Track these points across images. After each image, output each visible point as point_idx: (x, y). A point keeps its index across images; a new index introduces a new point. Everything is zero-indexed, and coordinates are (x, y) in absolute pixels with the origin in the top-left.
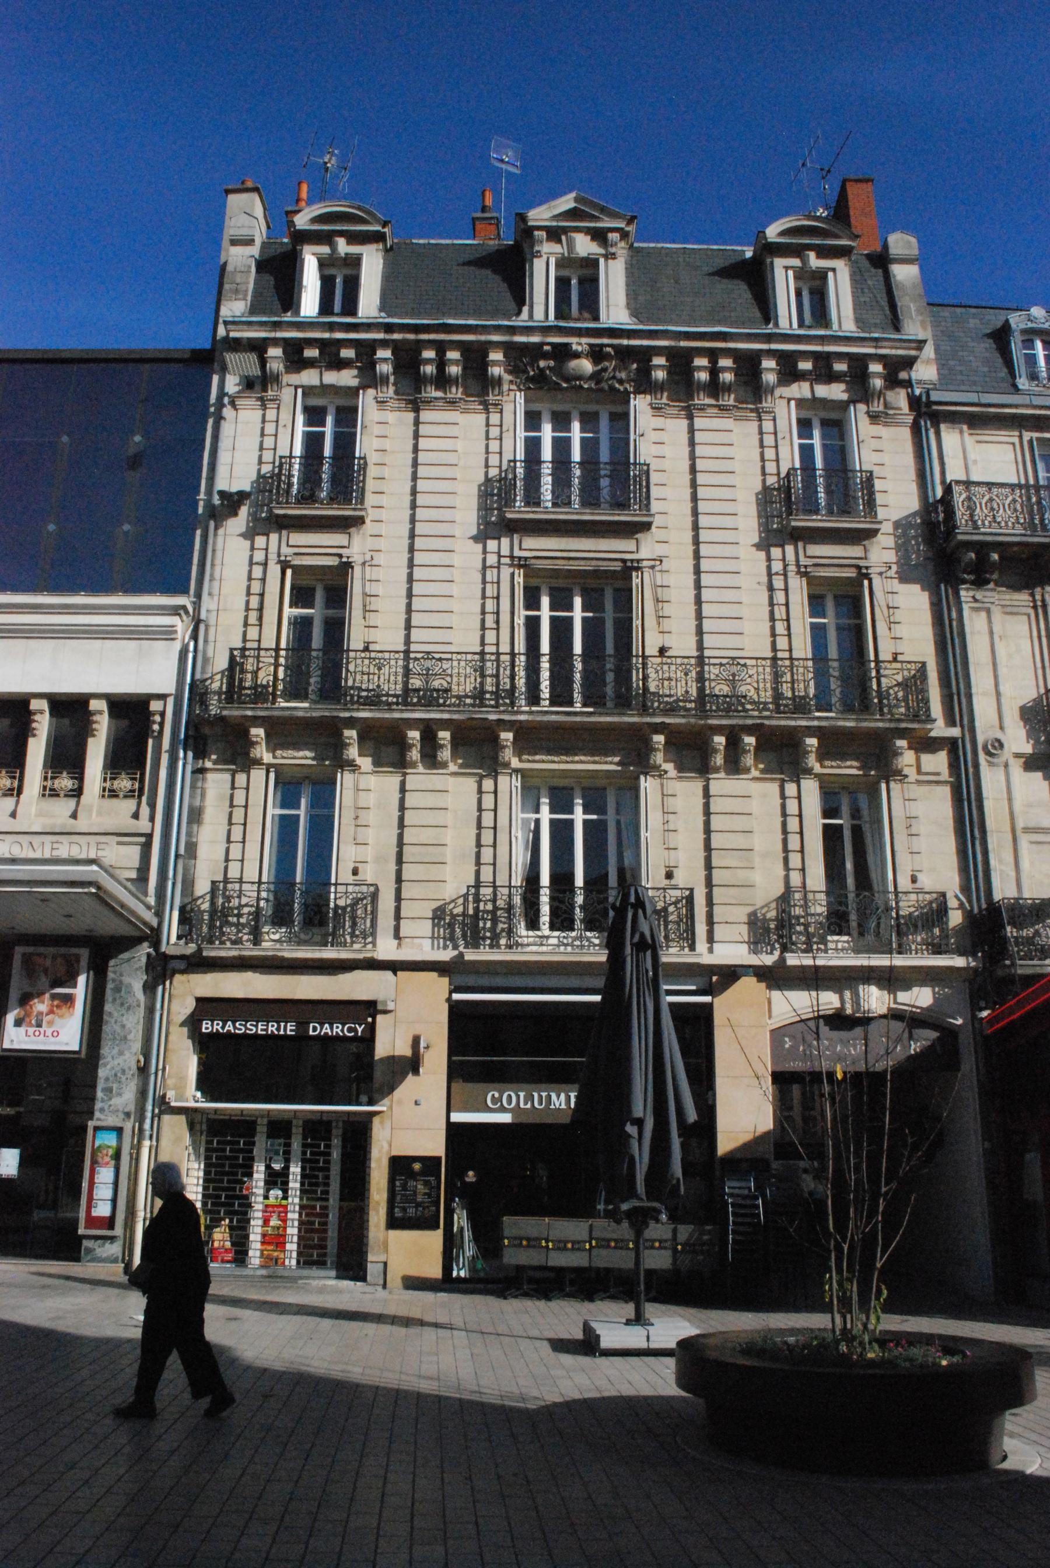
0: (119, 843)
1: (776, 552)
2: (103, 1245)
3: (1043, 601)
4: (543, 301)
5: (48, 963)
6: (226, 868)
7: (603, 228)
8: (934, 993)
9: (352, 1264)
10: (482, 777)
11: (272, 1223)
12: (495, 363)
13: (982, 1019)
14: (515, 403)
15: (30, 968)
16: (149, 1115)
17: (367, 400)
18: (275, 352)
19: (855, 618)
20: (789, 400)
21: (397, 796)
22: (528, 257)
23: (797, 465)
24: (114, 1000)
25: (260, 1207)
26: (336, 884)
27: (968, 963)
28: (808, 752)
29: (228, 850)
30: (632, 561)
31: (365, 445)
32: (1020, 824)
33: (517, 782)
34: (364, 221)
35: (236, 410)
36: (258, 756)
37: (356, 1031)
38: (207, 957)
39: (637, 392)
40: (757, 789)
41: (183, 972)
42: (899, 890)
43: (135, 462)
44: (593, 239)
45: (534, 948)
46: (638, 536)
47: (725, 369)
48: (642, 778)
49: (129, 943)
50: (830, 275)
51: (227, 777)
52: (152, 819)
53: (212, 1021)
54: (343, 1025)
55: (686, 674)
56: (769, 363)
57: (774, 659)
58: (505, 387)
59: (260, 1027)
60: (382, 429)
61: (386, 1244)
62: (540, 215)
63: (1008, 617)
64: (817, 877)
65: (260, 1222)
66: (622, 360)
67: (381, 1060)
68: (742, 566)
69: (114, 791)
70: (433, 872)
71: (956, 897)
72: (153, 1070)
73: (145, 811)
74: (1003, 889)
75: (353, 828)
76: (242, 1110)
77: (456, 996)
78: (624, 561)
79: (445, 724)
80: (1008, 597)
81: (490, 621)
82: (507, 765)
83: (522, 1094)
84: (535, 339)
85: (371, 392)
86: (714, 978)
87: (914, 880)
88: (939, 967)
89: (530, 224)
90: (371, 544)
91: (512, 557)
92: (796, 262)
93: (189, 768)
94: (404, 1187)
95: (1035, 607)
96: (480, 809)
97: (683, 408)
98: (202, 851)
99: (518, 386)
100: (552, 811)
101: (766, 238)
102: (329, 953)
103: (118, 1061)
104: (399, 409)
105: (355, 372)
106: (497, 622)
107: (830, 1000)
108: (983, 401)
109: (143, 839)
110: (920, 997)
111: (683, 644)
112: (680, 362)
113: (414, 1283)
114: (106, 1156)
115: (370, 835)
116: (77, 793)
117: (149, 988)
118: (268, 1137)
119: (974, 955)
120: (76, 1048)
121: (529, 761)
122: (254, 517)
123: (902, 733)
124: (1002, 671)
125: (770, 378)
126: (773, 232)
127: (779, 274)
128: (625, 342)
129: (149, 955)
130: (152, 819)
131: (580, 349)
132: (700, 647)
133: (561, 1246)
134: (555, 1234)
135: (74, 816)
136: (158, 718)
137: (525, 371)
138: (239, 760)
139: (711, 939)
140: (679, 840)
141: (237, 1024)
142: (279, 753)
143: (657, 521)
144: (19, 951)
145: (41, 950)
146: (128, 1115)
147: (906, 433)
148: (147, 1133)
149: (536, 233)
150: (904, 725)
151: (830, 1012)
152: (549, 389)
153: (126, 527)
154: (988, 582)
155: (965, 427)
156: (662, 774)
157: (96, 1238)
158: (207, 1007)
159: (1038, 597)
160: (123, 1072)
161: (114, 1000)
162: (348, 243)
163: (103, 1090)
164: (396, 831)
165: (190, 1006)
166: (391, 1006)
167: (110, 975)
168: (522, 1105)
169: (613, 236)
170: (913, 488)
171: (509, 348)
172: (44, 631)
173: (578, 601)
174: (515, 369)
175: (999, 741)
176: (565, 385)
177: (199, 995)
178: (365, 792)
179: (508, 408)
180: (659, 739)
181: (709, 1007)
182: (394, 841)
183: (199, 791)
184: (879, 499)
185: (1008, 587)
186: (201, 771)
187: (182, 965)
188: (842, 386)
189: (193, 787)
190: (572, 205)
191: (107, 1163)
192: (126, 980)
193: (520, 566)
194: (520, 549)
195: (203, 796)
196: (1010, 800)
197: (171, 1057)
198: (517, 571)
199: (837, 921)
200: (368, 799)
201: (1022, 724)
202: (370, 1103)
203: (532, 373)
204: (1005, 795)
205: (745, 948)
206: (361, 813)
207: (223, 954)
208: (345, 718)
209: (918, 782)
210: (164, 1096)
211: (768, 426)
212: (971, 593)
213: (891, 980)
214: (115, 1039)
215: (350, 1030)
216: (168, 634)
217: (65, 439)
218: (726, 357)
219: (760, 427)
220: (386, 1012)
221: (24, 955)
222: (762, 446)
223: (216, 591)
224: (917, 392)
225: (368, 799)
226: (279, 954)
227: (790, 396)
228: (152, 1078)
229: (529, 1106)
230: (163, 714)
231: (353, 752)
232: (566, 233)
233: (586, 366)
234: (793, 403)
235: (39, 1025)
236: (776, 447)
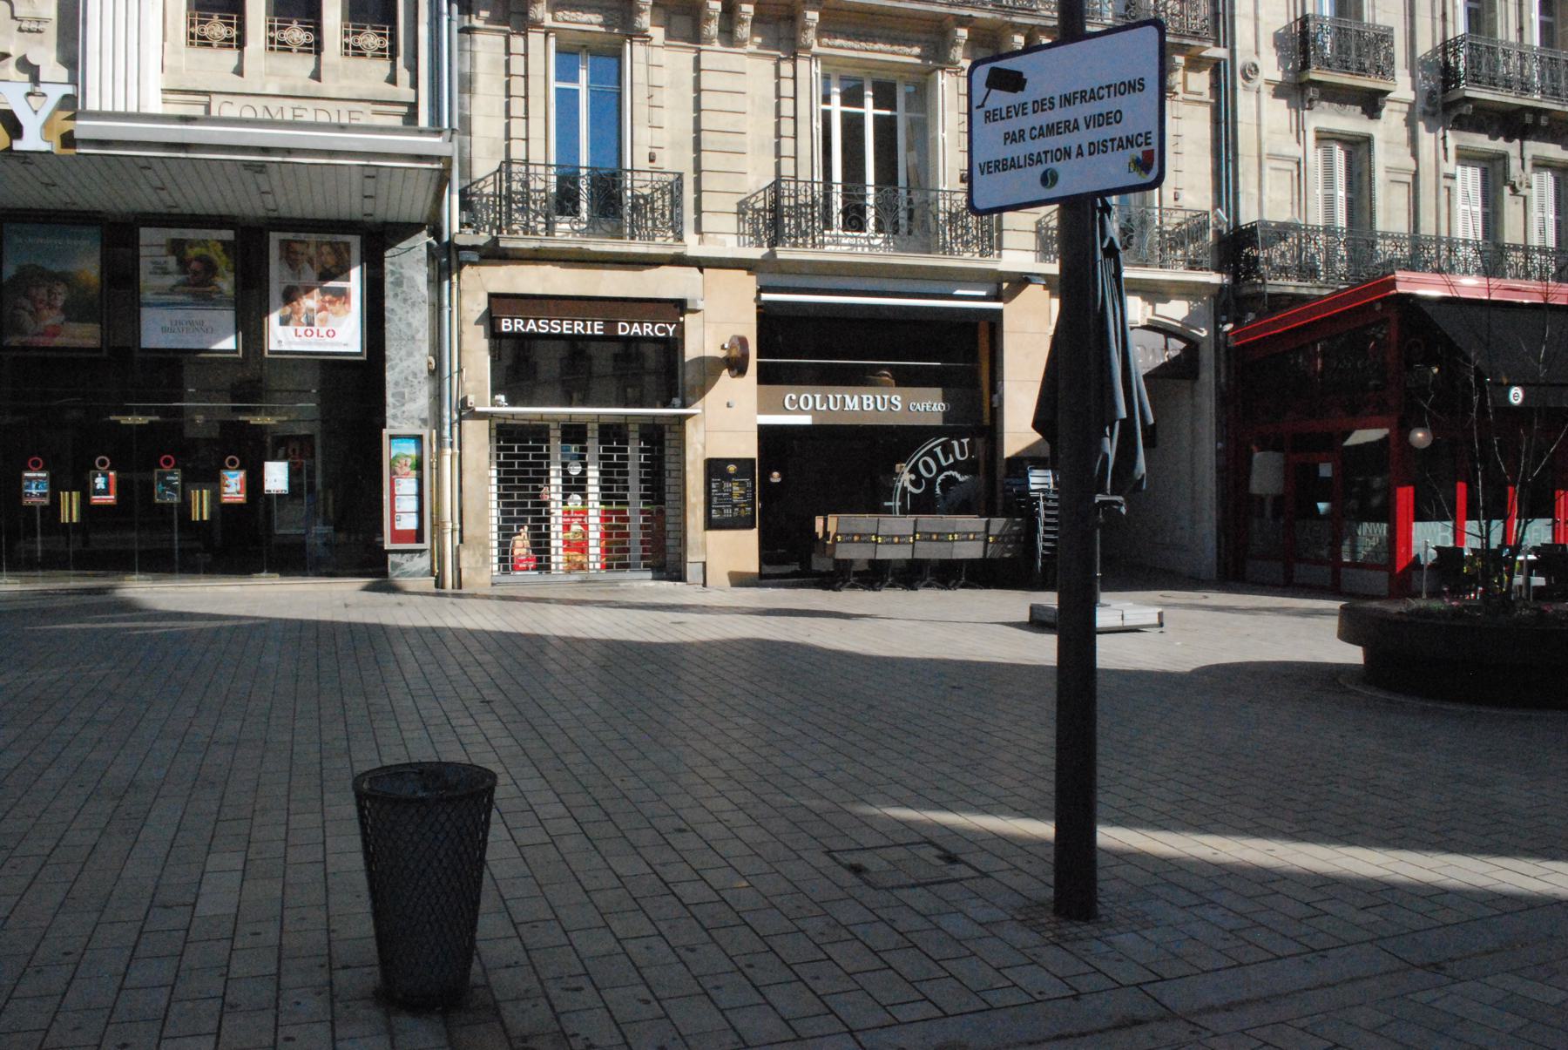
5: (312, 251)
6: (508, 148)
9: (669, 566)
10: (780, 59)
15: (290, 255)
16: (447, 421)
21: (691, 75)
24: (396, 295)
25: (559, 513)
26: (632, 171)
29: (508, 127)
32: (1265, 150)
33: (817, 69)
38: (505, 249)
40: (749, 64)
41: (473, 264)
45: (832, 248)
49: (406, 230)
51: (501, 39)
52: (415, 84)
54: (654, 324)
61: (704, 544)
67: (691, 361)
70: (733, 162)
72: (447, 373)
73: (403, 75)
76: (542, 415)
77: (765, 297)
83: (818, 396)
86: (1005, 285)
94: (720, 488)
96: (778, 96)
98: (478, 125)
102: (638, 247)
103: (405, 366)
109: (405, 109)
110: (1176, 311)
113: (739, 580)
114: (406, 467)
117: (436, 282)
120: (358, 350)
129: (429, 245)
130: (415, 84)
135: (239, 71)
138: (513, 19)
142: (559, 14)
144: (275, 238)
145: (302, 236)
146: (424, 421)
148: (448, 440)
157: (403, 552)
158: (500, 303)
160: (415, 375)
161: (396, 295)
164: (692, 115)
165: (483, 305)
166: (700, 305)
167: (388, 267)
177: (492, 291)
180: (963, 33)
181: (999, 313)
182: (691, 126)
186: (468, 31)
187: (475, 257)
189: (461, 50)
192: (407, 272)
195: (473, 59)
197: (466, 358)
202: (684, 406)
205: (1032, 255)
206: (656, 91)
207: (523, 245)
210: (464, 401)
214: (401, 339)
215: (660, 330)
220: (695, 311)
221: (282, 242)
226: (585, 247)
235: (310, 324)
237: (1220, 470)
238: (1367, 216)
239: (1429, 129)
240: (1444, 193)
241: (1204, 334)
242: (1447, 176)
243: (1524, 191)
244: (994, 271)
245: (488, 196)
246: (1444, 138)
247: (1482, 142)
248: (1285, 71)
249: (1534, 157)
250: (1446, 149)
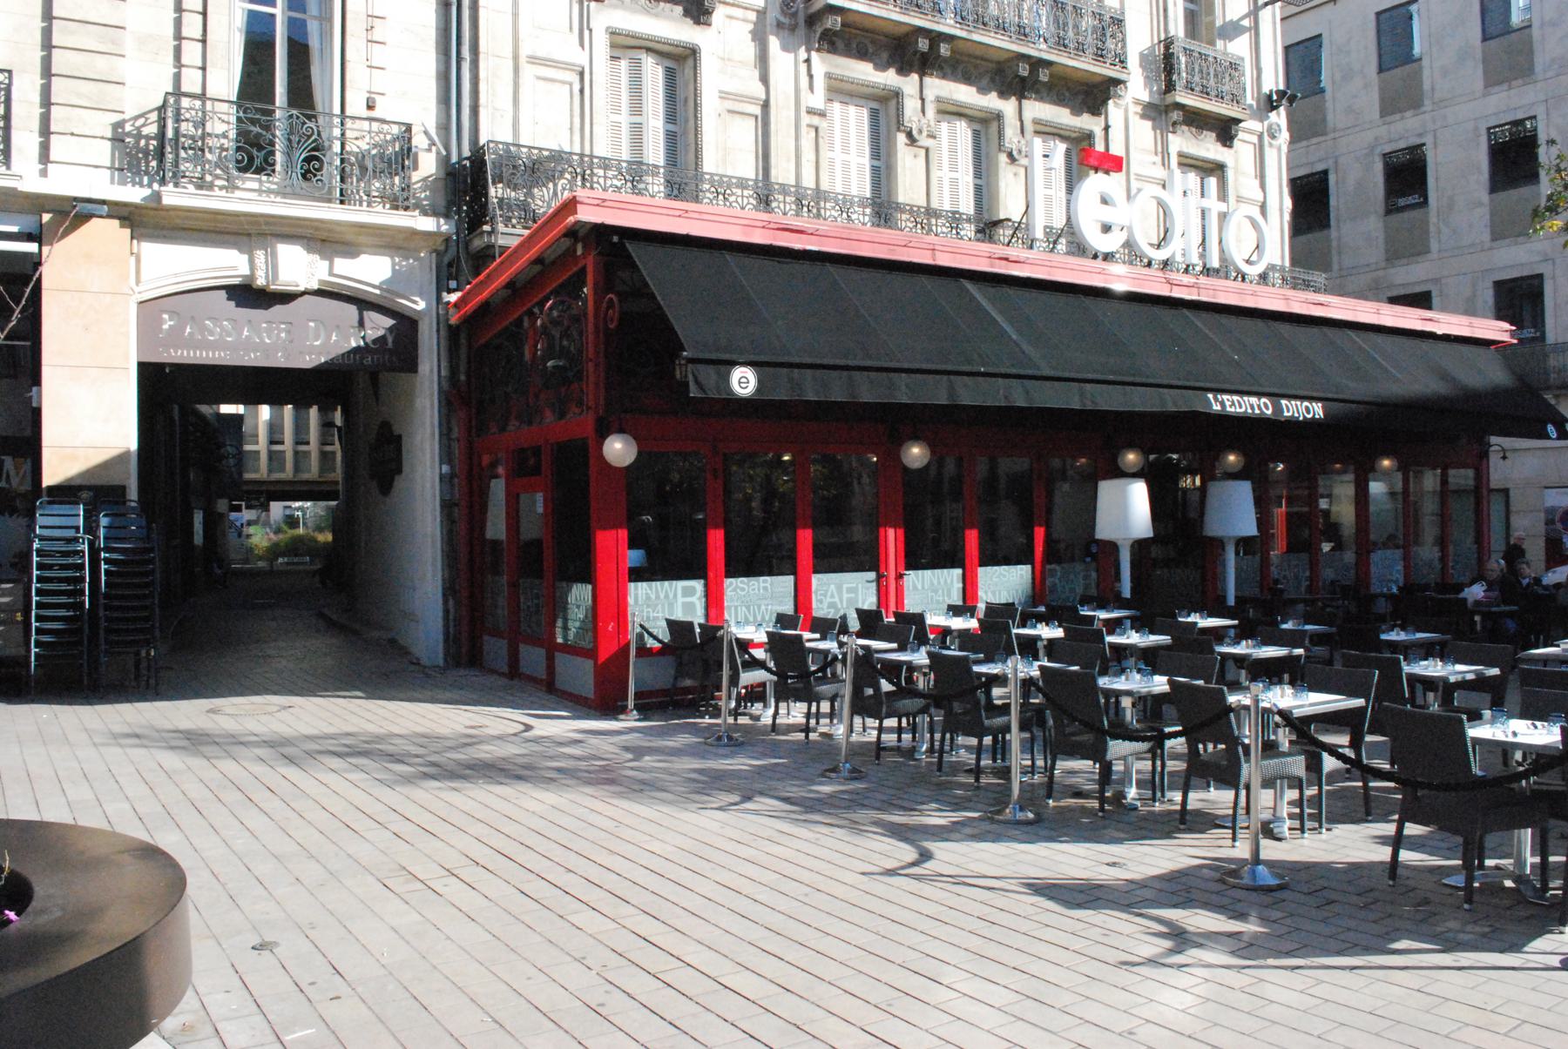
8: (394, 265)
13: (448, 303)
27: (439, 226)
32: (524, 51)
42: (348, 113)
71: (426, 133)
74: (494, 129)
107: (229, 263)
110: (370, 271)
119: (447, 216)
139: (45, 156)
151: (236, 281)
181: (36, 262)
199: (253, 154)
213: (323, 240)
237: (447, 506)
238: (692, 156)
239: (785, 48)
240: (808, 139)
241: (421, 305)
242: (811, 112)
243: (924, 141)
244: (15, 189)
245: (148, 138)
246: (808, 61)
247: (863, 71)
248: (1151, 91)
249: (939, 100)
250: (811, 76)
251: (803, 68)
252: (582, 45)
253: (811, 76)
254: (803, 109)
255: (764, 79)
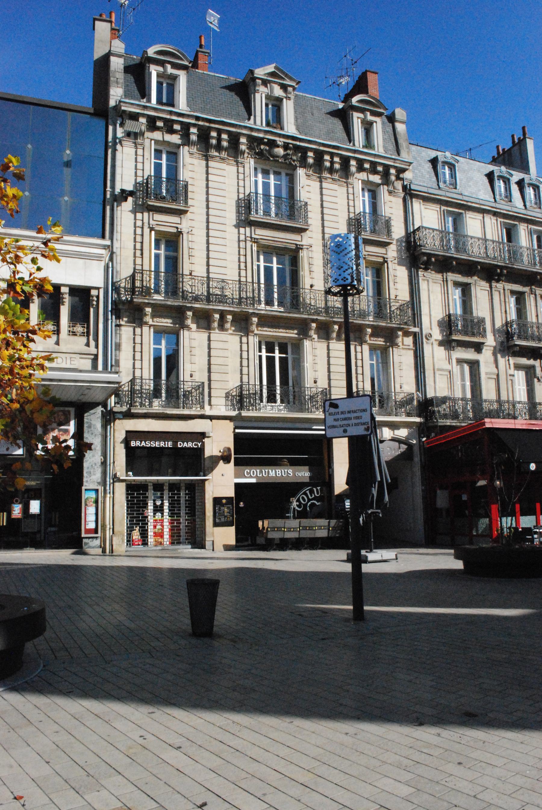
0: (81, 358)
1: (139, 216)
2: (93, 541)
3: (446, 279)
4: (260, 115)
7: (285, 84)
10: (242, 336)
11: (157, 527)
12: (243, 144)
14: (250, 163)
16: (108, 483)
17: (184, 151)
18: (143, 120)
19: (174, 252)
20: (151, 140)
22: (253, 91)
23: (153, 174)
24: (88, 432)
25: (152, 521)
28: (253, 324)
30: (300, 245)
31: (184, 175)
32: (436, 367)
34: (182, 59)
35: (122, 146)
36: (147, 321)
37: (198, 445)
39: (300, 167)
43: (68, 164)
44: (281, 88)
46: (302, 234)
47: (336, 162)
48: (305, 340)
49: (93, 405)
50: (375, 124)
51: (131, 329)
52: (97, 347)
53: (136, 441)
54: (193, 443)
55: (202, 285)
56: (353, 163)
57: (240, 281)
58: (246, 155)
59: (157, 444)
60: (191, 166)
61: (213, 533)
62: (260, 72)
63: (434, 284)
64: (148, 373)
65: (152, 527)
66: (295, 151)
68: (226, 235)
69: (74, 332)
73: (92, 343)
75: (189, 356)
78: (296, 245)
79: (230, 312)
80: (434, 275)
81: (243, 265)
82: (253, 332)
83: (258, 471)
84: (261, 135)
85: (186, 148)
87: (191, 376)
88: (295, 418)
89: (255, 75)
90: (191, 223)
91: (251, 238)
92: (362, 116)
93: (114, 324)
94: (220, 510)
95: (443, 281)
96: (241, 350)
97: (319, 177)
98: (122, 363)
99: (251, 156)
100: (280, 353)
101: (351, 103)
104: (199, 159)
105: (179, 137)
106: (246, 267)
108: (430, 192)
109: (93, 357)
110: (403, 433)
111: (200, 271)
112: (319, 156)
113: (227, 548)
115: (196, 359)
116: (58, 332)
117: (105, 427)
118: (169, 491)
121: (261, 330)
122: (135, 203)
123: (400, 329)
124: (432, 306)
125: (353, 169)
126: (151, 52)
127: (355, 119)
128: (298, 143)
129: (102, 411)
130: (97, 347)
131: (280, 144)
132: (208, 272)
133: (289, 530)
134: (287, 525)
135: (57, 343)
136: (95, 299)
137: (254, 149)
140: (318, 367)
141: (147, 442)
143: (310, 228)
147: (400, 201)
149: (257, 81)
150: (402, 326)
152: (265, 159)
153: (66, 198)
154: (428, 269)
155: (421, 201)
156: (312, 340)
158: (131, 435)
159: (445, 277)
161: (88, 432)
162: (172, 68)
163: (87, 473)
165: (123, 436)
166: (211, 435)
168: (258, 475)
169: (290, 89)
170: (403, 226)
171: (250, 138)
172: (81, 255)
173: (275, 259)
174: (250, 148)
175: (430, 334)
176: (271, 159)
177: (128, 429)
178: (193, 339)
179: (247, 166)
180: (314, 325)
182: (207, 363)
183: (118, 335)
184: (190, 195)
185: (436, 272)
188: (379, 177)
190: (273, 70)
191: (92, 505)
192: (93, 422)
193: (255, 242)
194: (255, 234)
196: (433, 357)
198: (253, 244)
200: (318, 352)
201: (438, 328)
202: (204, 476)
203: (257, 151)
204: (431, 356)
208: (189, 307)
209: (403, 349)
211: (140, 152)
212: (423, 273)
215: (195, 445)
216: (99, 258)
217: (29, 146)
218: (225, 134)
219: (136, 152)
222: (136, 161)
223: (119, 238)
224: (405, 183)
225: (194, 344)
227: (152, 138)
228: (108, 467)
229: (261, 475)
230: (98, 297)
231: (189, 322)
232: (270, 83)
233: (280, 151)
234: (153, 142)
236: (354, 200)
238: (479, 392)
239: (502, 357)
240: (510, 382)
242: (510, 375)
246: (508, 360)
247: (524, 361)
250: (509, 364)
251: (507, 362)
252: (449, 363)
253: (509, 364)
254: (508, 375)
255: (497, 367)
